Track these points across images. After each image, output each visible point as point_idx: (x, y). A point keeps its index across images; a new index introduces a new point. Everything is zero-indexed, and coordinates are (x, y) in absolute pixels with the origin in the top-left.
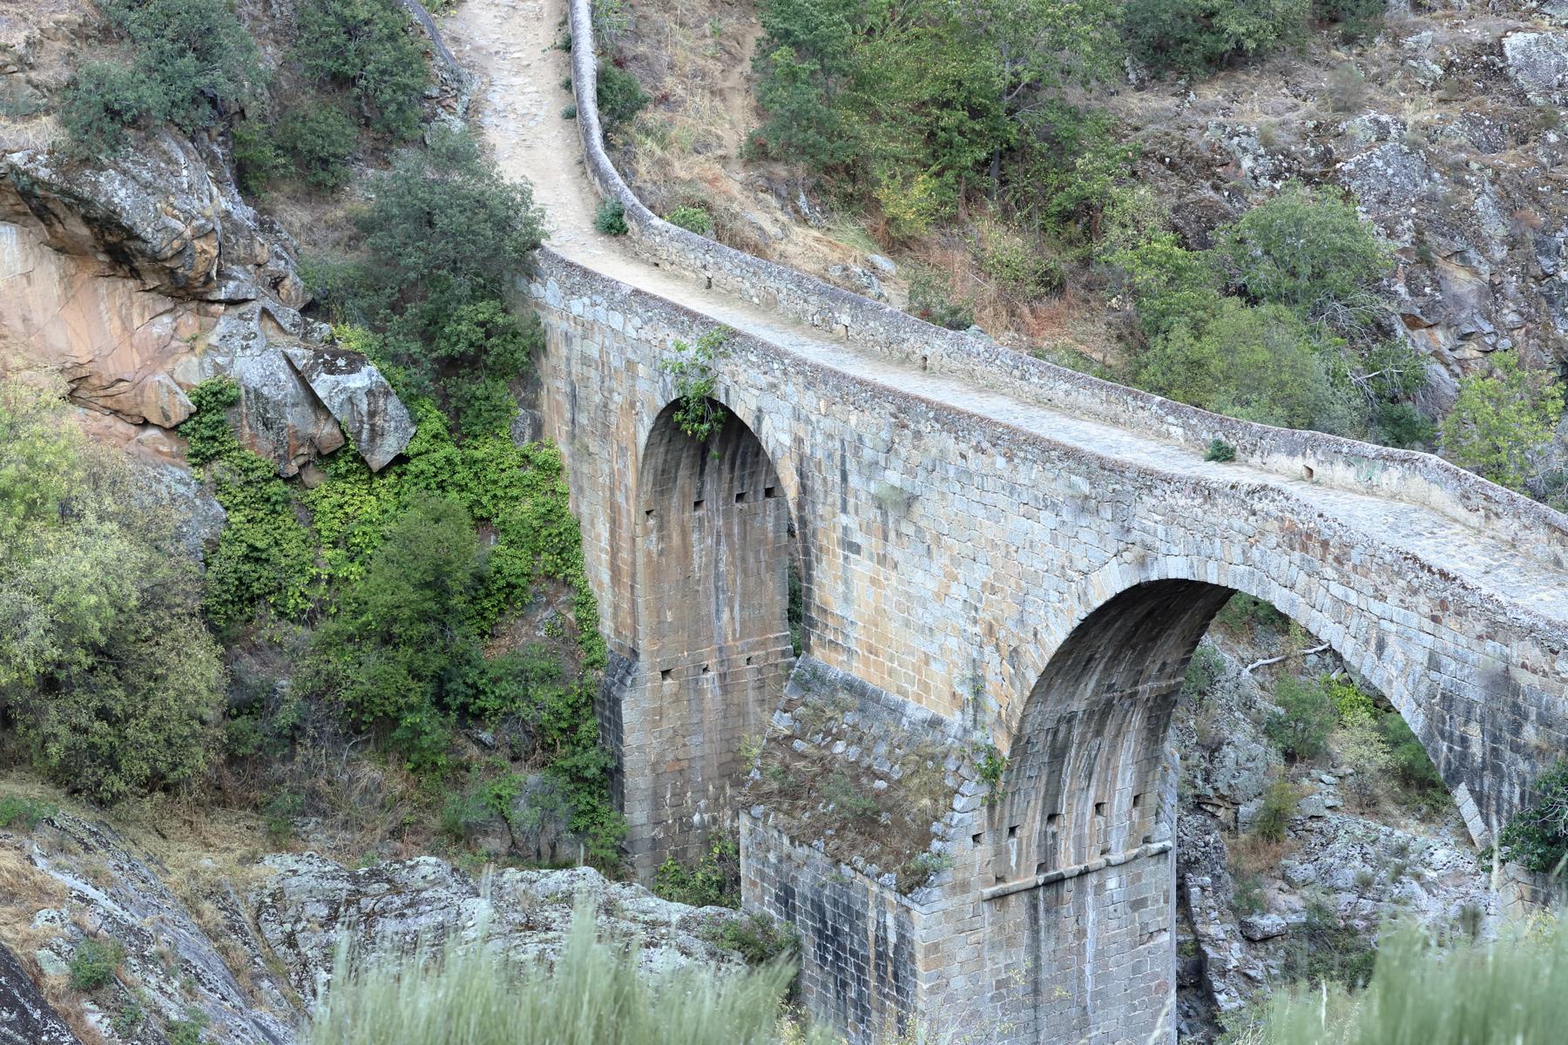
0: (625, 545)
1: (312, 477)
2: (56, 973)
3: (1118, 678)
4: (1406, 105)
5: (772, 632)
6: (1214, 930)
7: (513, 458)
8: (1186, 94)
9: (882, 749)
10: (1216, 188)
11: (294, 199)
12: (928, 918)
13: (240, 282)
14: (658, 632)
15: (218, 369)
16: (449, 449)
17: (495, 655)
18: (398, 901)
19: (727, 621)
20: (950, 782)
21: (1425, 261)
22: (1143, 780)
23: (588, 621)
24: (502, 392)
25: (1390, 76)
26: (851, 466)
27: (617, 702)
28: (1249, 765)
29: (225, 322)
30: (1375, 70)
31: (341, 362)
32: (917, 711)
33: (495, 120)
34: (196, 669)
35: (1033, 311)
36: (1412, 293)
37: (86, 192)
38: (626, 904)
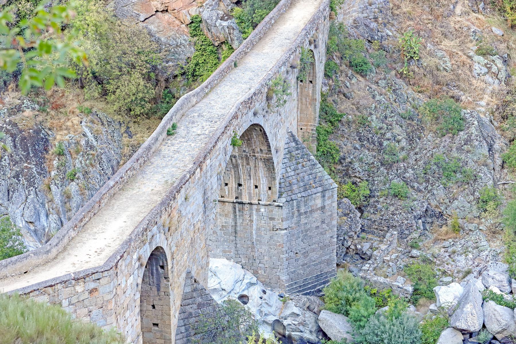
5: (310, 122)
15: (200, 12)
28: (462, 208)
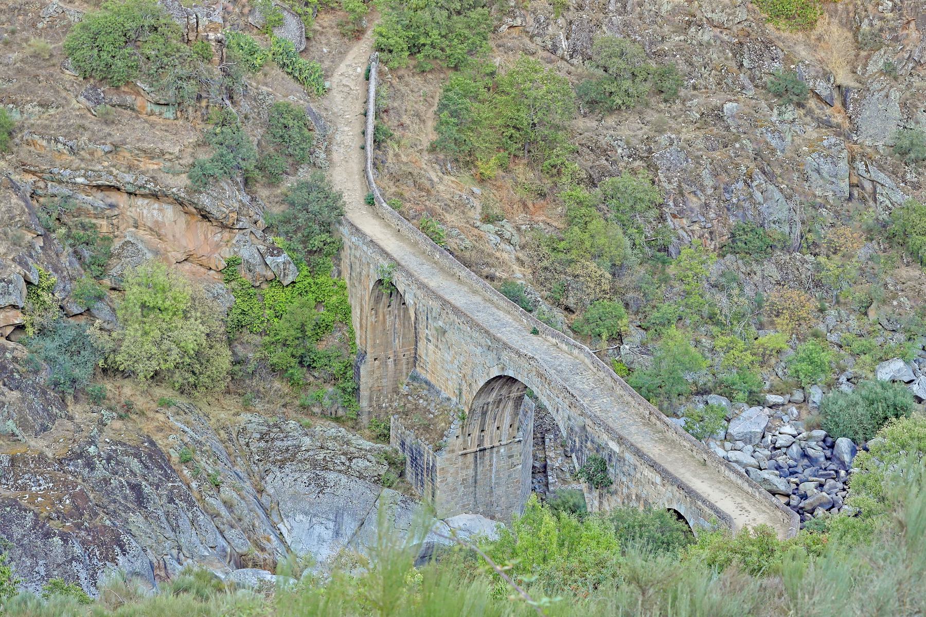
0: (364, 318)
1: (264, 286)
2: (175, 457)
3: (504, 392)
4: (684, 130)
6: (552, 454)
7: (331, 282)
8: (601, 121)
9: (433, 405)
10: (607, 160)
11: (263, 186)
12: (441, 461)
13: (245, 222)
14: (374, 346)
15: (235, 252)
16: (310, 280)
17: (321, 348)
18: (282, 435)
19: (397, 343)
20: (451, 419)
21: (681, 194)
22: (513, 420)
23: (352, 338)
24: (329, 261)
25: (680, 117)
26: (429, 316)
27: (359, 368)
29: (238, 236)
30: (674, 114)
31: (275, 252)
32: (444, 394)
33: (336, 147)
34: (223, 360)
35: (534, 204)
36: (675, 205)
37: (196, 201)
38: (353, 442)
